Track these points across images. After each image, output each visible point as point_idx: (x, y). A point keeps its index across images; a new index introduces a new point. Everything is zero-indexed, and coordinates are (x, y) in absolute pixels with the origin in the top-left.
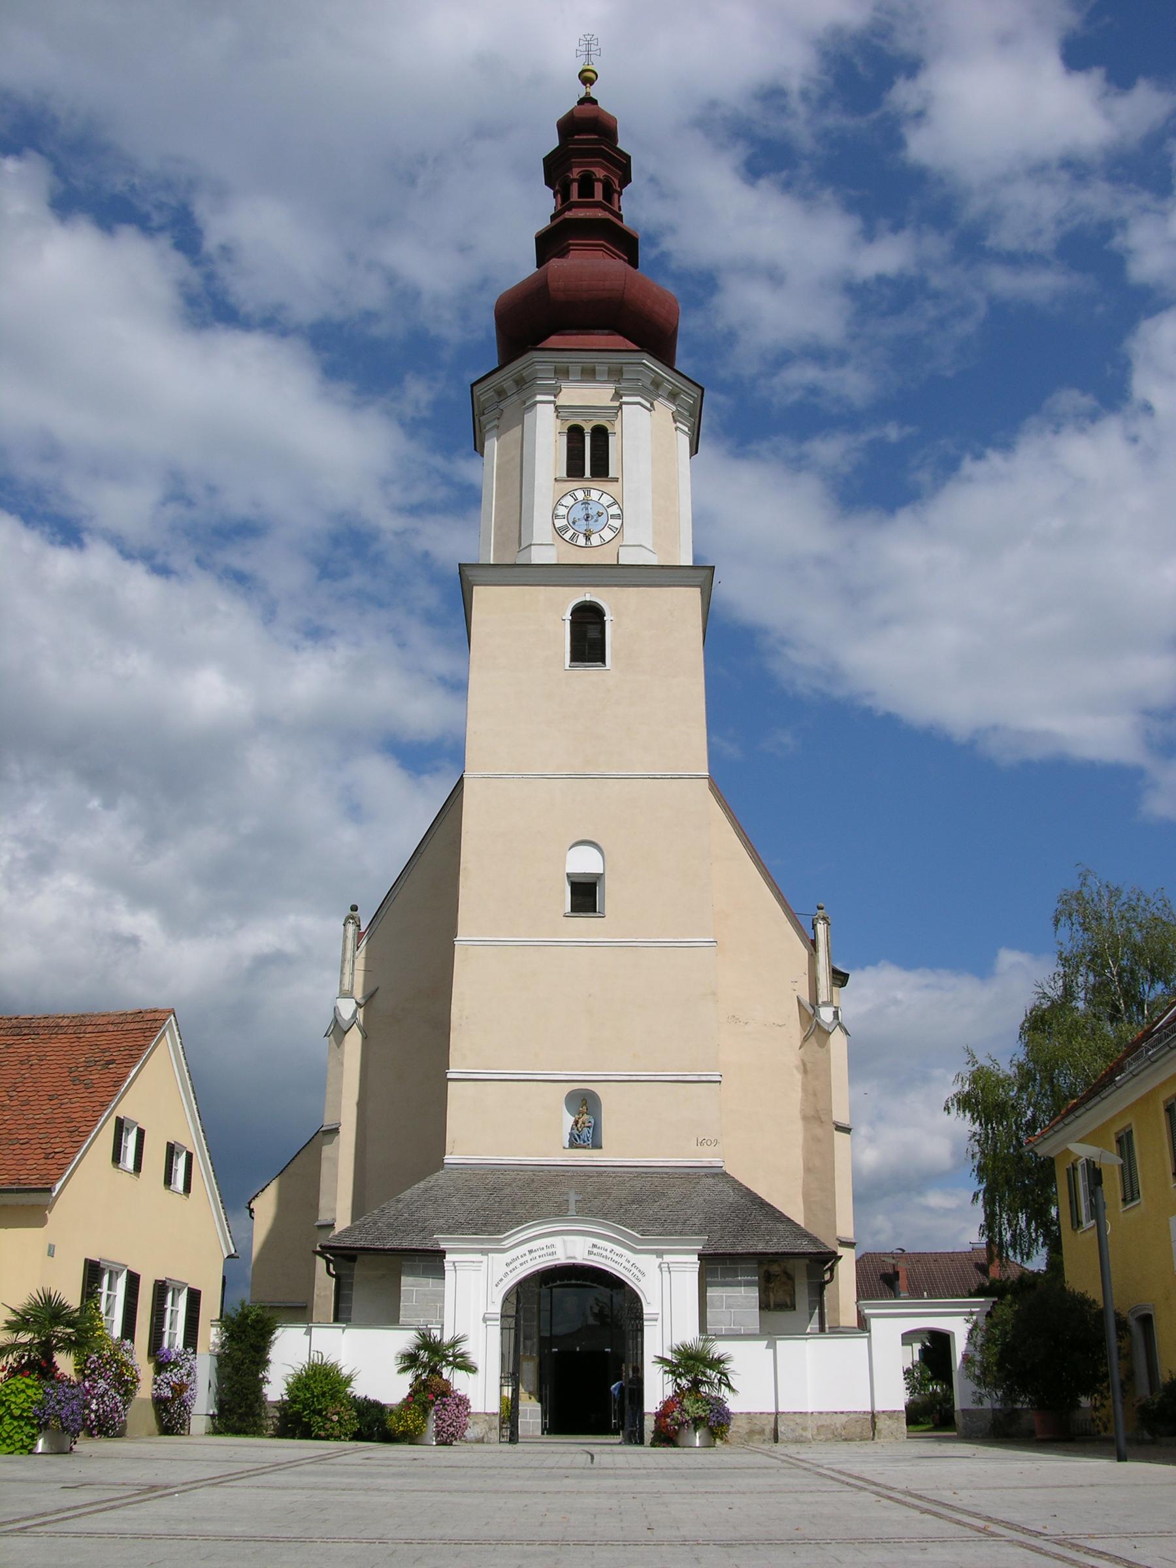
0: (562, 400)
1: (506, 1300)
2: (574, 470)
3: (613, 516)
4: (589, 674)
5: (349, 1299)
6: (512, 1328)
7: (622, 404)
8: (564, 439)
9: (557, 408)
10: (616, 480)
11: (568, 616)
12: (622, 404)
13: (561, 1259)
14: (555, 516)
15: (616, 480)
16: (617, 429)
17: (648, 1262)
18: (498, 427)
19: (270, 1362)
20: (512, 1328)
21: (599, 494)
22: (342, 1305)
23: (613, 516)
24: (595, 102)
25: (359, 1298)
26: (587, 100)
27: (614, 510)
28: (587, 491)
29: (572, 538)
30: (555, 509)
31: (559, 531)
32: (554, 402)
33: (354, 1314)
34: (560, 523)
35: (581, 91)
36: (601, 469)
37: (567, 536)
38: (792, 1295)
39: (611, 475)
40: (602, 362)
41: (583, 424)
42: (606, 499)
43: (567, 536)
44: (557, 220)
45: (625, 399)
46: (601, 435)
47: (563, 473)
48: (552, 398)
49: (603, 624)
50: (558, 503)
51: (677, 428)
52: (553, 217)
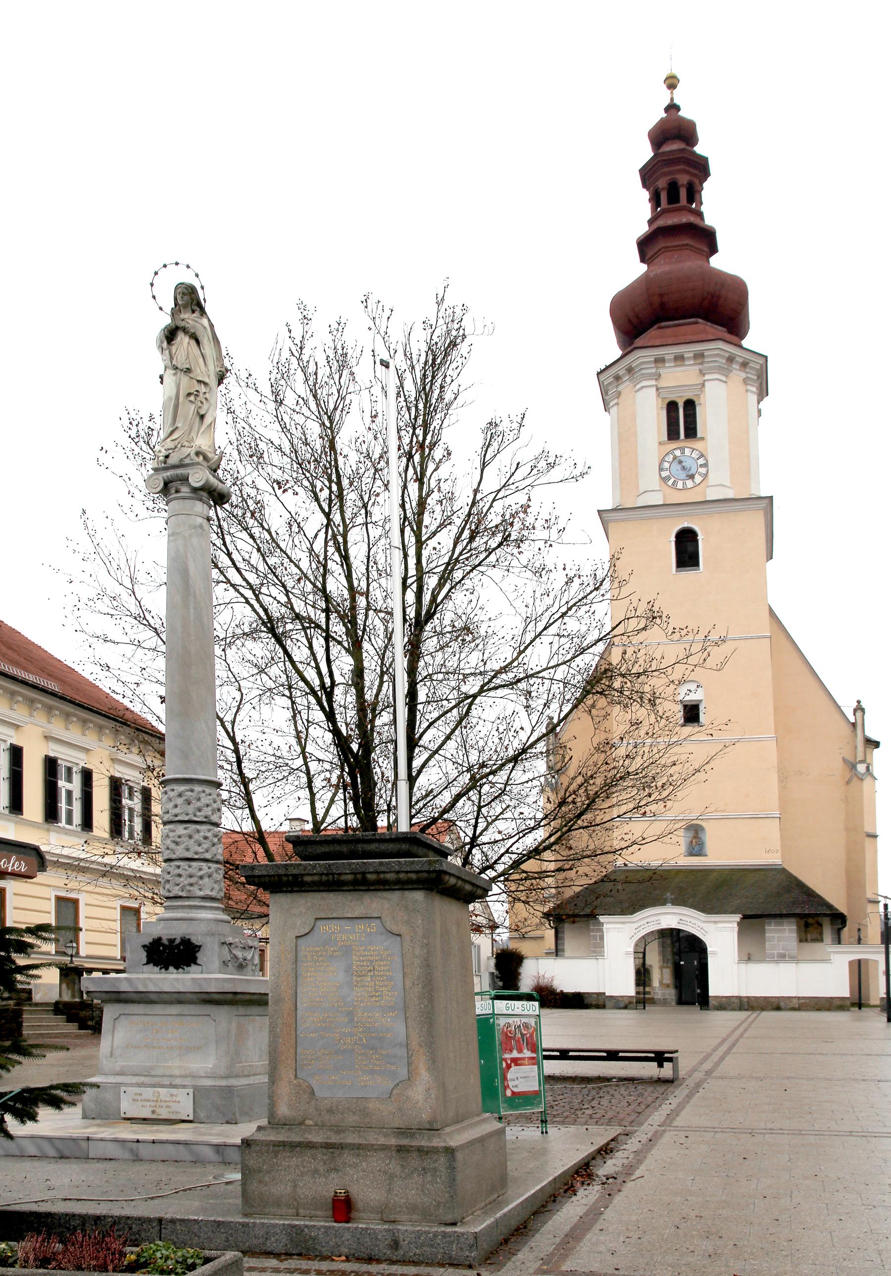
0: (662, 383)
1: (636, 945)
2: (673, 434)
3: (701, 466)
4: (689, 575)
5: (563, 939)
6: (477, 994)
7: (704, 381)
8: (664, 412)
9: (657, 389)
10: (702, 439)
11: (673, 539)
12: (704, 381)
13: (664, 926)
14: (661, 469)
15: (702, 439)
16: (702, 401)
17: (706, 926)
18: (617, 404)
19: (802, 940)
20: (477, 994)
21: (688, 450)
22: (560, 935)
23: (701, 466)
24: (677, 108)
25: (569, 944)
26: (672, 108)
27: (701, 461)
28: (682, 449)
29: (673, 484)
30: (660, 465)
31: (665, 480)
32: (656, 386)
33: (566, 954)
34: (664, 474)
35: (664, 98)
36: (691, 432)
37: (670, 483)
38: (821, 934)
39: (699, 435)
40: (688, 350)
41: (678, 400)
42: (695, 455)
43: (670, 483)
44: (656, 225)
45: (707, 377)
46: (690, 405)
47: (665, 438)
48: (653, 382)
49: (697, 541)
50: (663, 460)
51: (747, 391)
52: (651, 222)
